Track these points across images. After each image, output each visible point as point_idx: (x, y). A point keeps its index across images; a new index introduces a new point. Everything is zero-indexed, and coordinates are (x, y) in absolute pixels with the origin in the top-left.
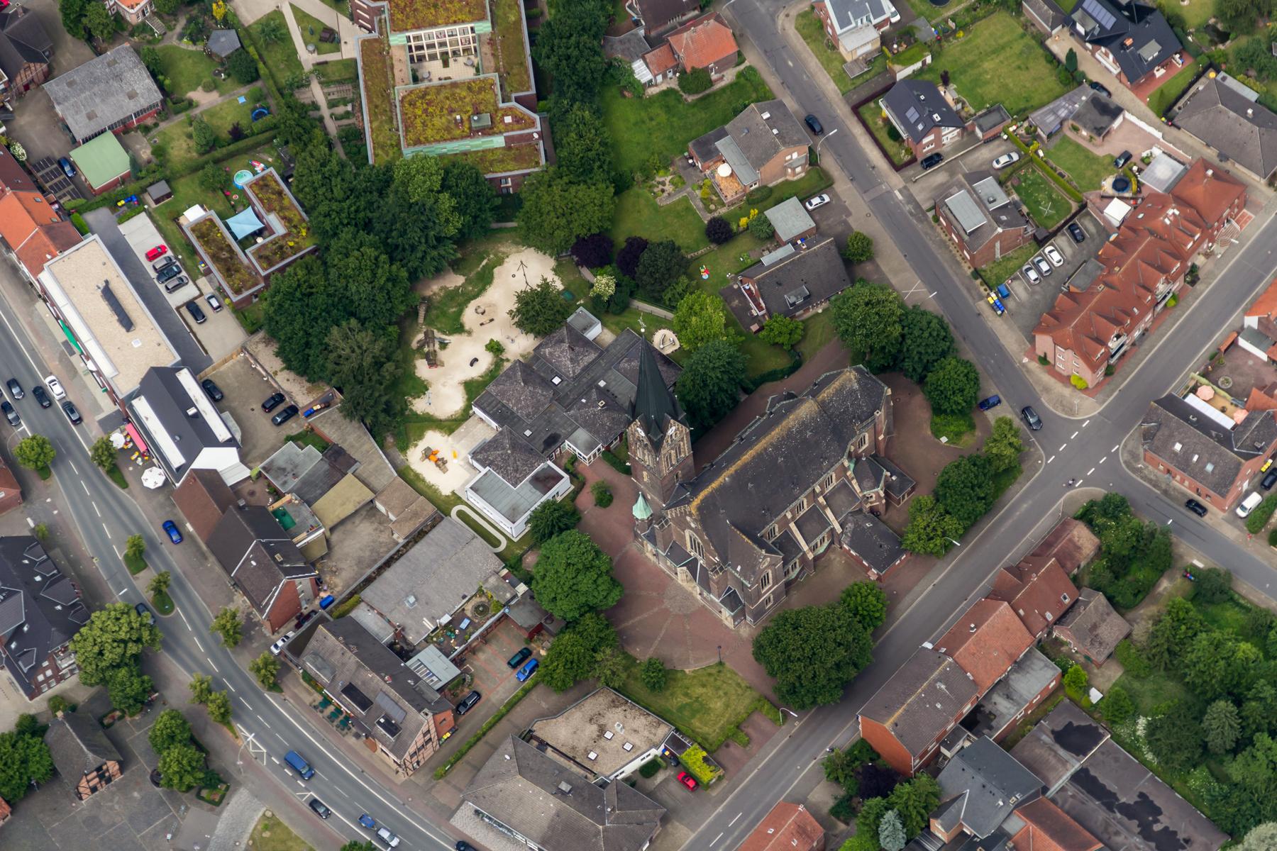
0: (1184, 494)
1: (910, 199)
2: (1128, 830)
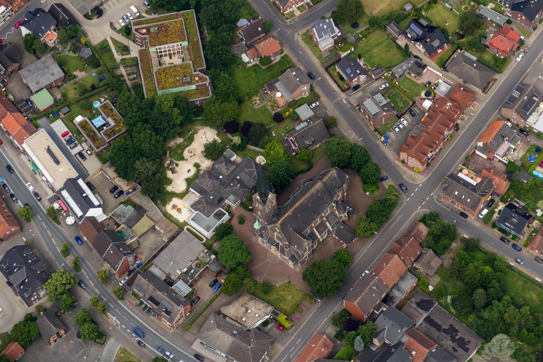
1: (349, 102)
2: (446, 339)
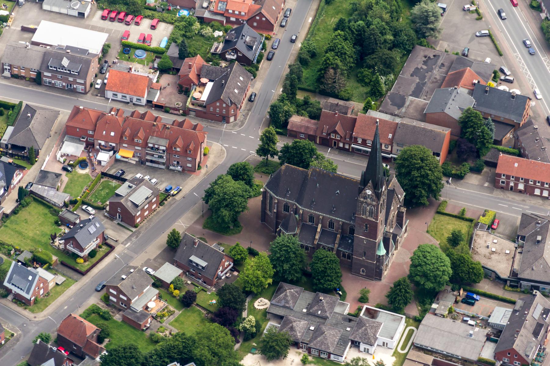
0: (247, 104)
1: (129, 239)
2: (431, 76)
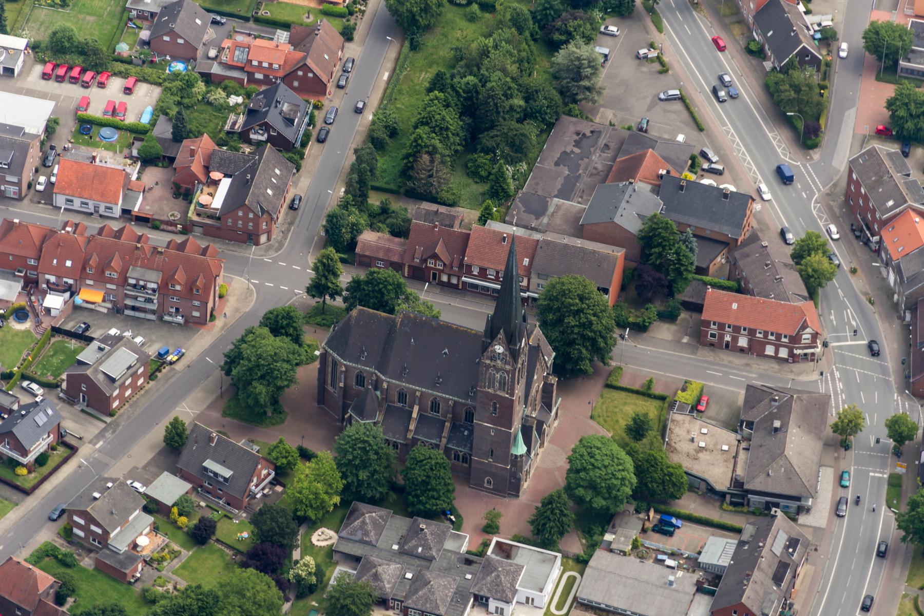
0: (287, 214)
1: (101, 435)
2: (588, 164)
